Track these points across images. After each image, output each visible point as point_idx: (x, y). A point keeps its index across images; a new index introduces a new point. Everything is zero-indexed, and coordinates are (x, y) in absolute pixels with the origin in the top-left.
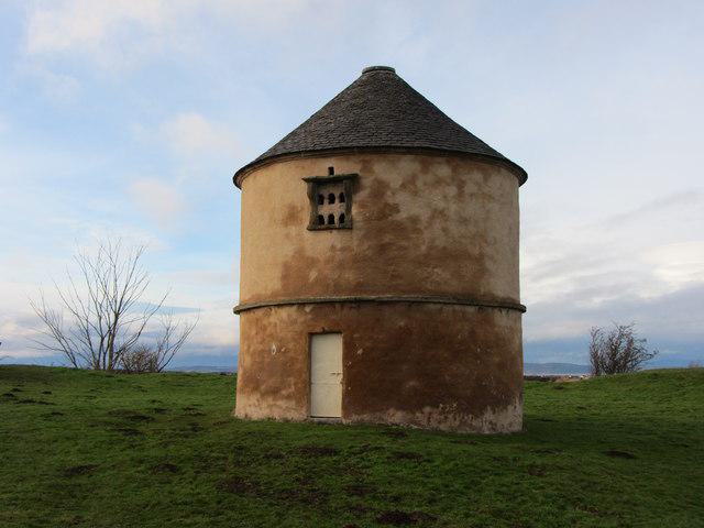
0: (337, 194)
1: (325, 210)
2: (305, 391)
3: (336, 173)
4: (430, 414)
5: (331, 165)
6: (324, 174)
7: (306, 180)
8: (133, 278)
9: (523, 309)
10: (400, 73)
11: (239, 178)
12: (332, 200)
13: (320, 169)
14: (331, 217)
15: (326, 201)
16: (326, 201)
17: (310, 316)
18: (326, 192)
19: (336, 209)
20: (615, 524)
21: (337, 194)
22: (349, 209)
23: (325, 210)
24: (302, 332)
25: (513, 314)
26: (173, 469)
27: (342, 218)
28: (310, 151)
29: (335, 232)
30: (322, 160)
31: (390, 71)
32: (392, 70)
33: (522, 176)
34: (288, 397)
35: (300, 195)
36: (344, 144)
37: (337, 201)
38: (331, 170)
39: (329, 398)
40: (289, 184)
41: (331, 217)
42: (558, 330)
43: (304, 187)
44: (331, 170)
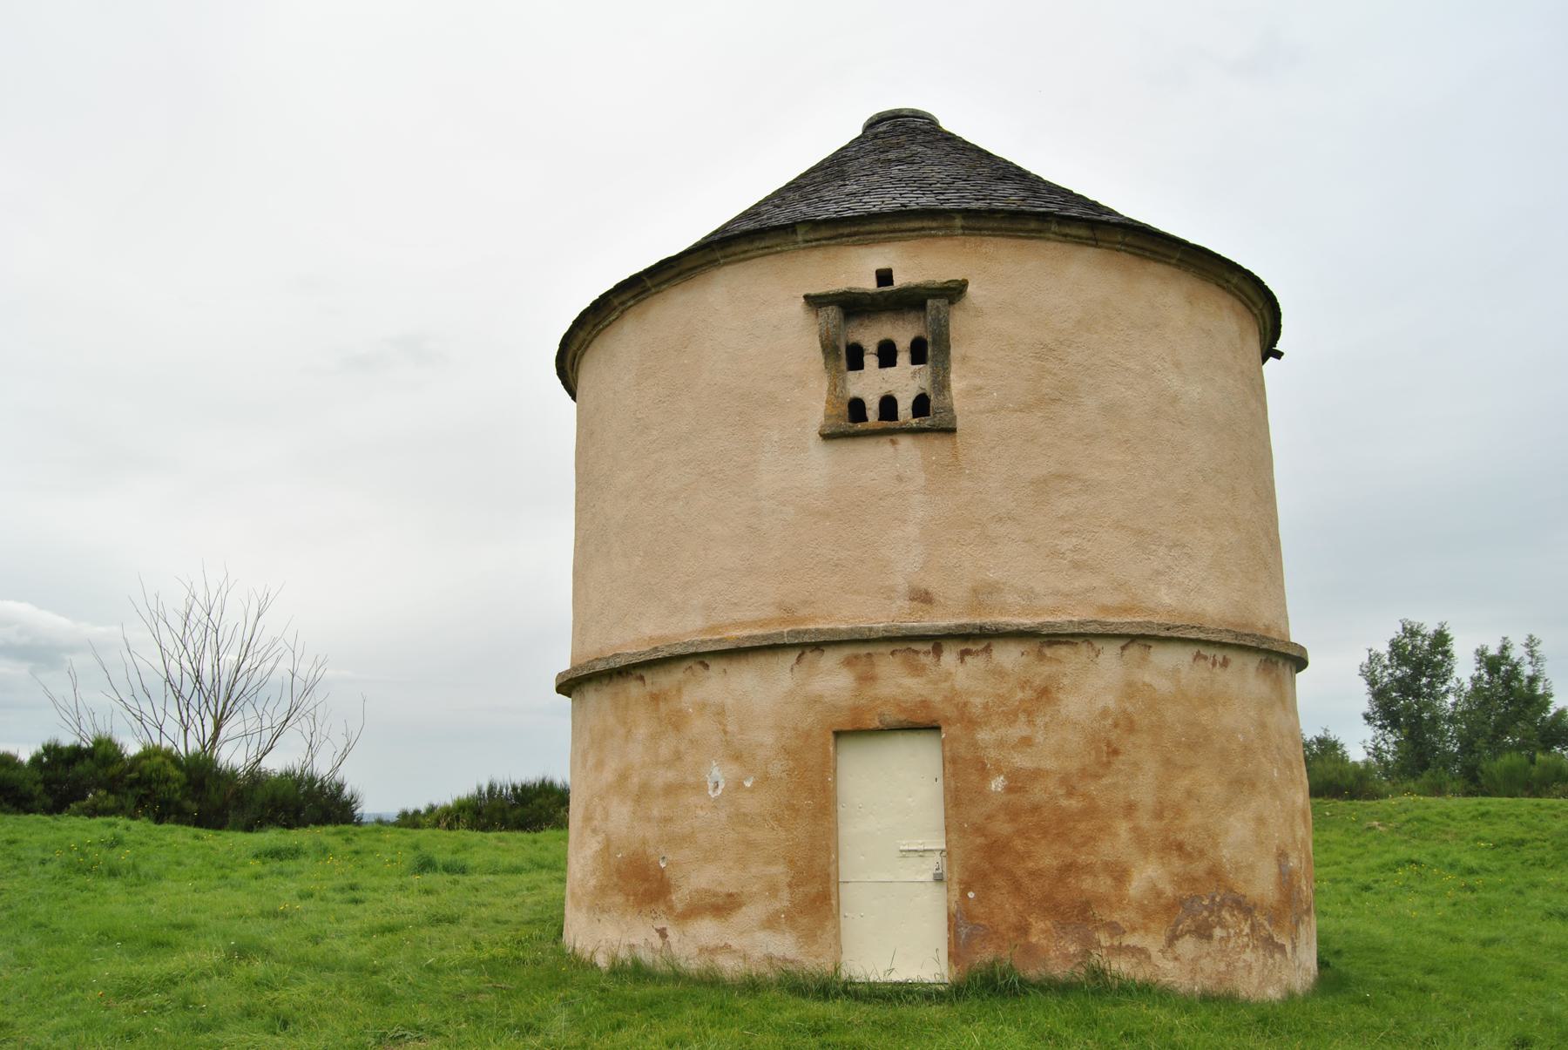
0: (903, 340)
1: (870, 384)
2: (815, 896)
3: (900, 280)
4: (1195, 960)
5: (883, 265)
6: (870, 284)
8: (248, 661)
11: (567, 686)
12: (887, 355)
13: (856, 269)
14: (888, 406)
15: (871, 361)
16: (871, 361)
18: (870, 336)
19: (905, 381)
22: (941, 384)
23: (870, 384)
24: (1216, 845)
26: (1018, 889)
27: (921, 405)
29: (905, 442)
30: (862, 251)
33: (1260, 308)
34: (771, 923)
35: (800, 338)
37: (903, 358)
38: (884, 277)
39: (897, 931)
40: (768, 313)
41: (888, 406)
42: (946, 974)
44: (884, 277)
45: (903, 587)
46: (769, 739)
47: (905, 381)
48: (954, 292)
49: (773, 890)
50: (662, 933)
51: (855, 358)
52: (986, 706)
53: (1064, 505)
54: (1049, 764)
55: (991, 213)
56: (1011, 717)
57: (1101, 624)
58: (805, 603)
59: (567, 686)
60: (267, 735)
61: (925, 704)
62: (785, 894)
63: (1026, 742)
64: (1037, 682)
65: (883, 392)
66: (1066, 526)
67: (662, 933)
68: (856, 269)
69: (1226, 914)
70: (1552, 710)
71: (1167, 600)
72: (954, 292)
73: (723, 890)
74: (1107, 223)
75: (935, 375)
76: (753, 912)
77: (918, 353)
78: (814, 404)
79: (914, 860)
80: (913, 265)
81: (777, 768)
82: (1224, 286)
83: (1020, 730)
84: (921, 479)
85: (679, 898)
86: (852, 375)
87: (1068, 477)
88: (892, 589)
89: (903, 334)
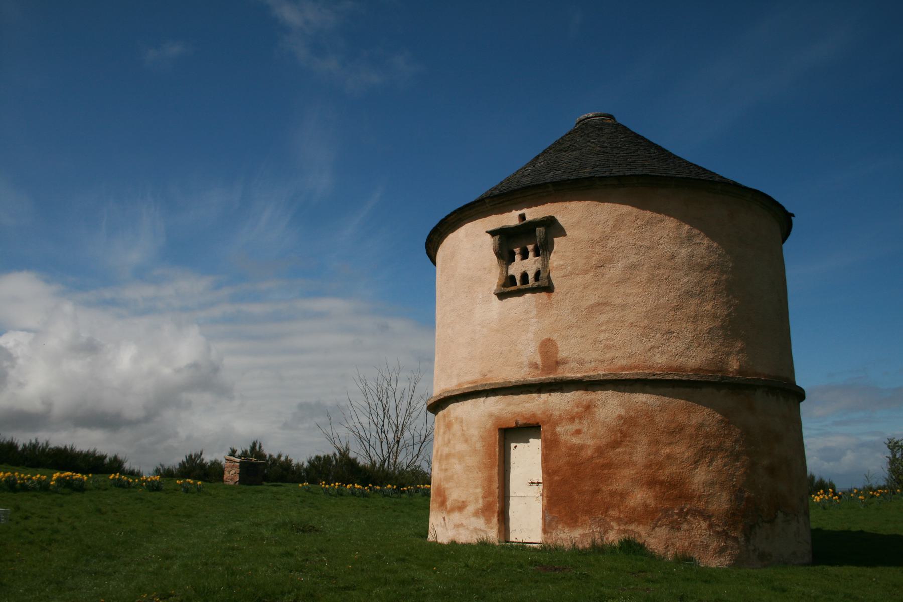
1: (517, 268)
3: (528, 218)
7: (493, 233)
9: (800, 395)
13: (511, 219)
14: (524, 276)
19: (529, 265)
38: (522, 217)
39: (528, 523)
41: (524, 276)
44: (522, 217)
45: (526, 363)
46: (476, 433)
49: (476, 500)
50: (444, 518)
52: (560, 416)
53: (603, 318)
54: (591, 442)
55: (577, 181)
56: (572, 419)
57: (615, 375)
58: (490, 371)
60: (417, 448)
61: (534, 416)
62: (481, 501)
63: (578, 432)
64: (585, 403)
66: (604, 328)
67: (444, 518)
68: (511, 219)
69: (334, 463)
71: (659, 361)
73: (461, 499)
75: (543, 261)
76: (471, 508)
79: (535, 487)
81: (479, 446)
83: (576, 426)
84: (534, 312)
85: (449, 504)
87: (605, 304)
88: (522, 363)
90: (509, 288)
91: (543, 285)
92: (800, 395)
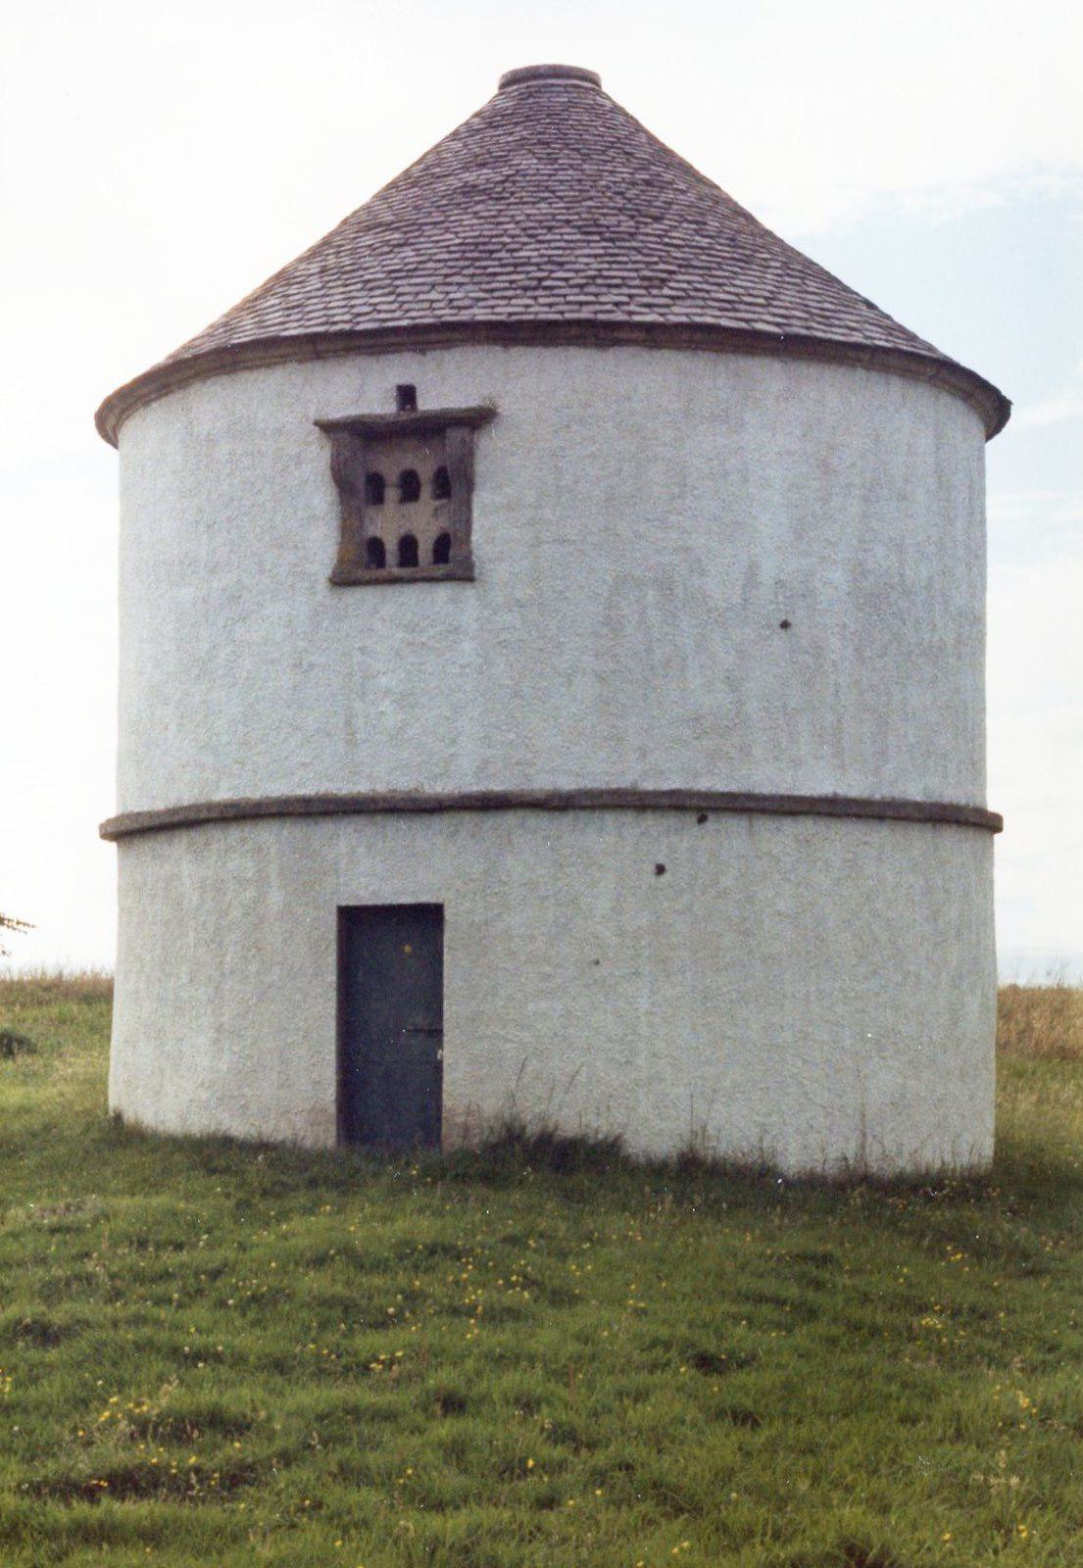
0: (426, 473)
1: (388, 523)
5: (405, 380)
7: (328, 428)
9: (991, 824)
10: (621, 88)
11: (128, 832)
12: (410, 489)
13: (363, 390)
14: (408, 545)
15: (392, 494)
16: (392, 494)
17: (1063, 1157)
18: (390, 465)
19: (424, 520)
20: (135, 1562)
21: (426, 473)
23: (388, 523)
25: (952, 843)
27: (443, 547)
28: (341, 334)
31: (578, 83)
32: (592, 79)
36: (448, 315)
37: (426, 492)
38: (407, 395)
41: (408, 545)
43: (318, 456)
44: (407, 395)
47: (424, 520)
48: (479, 419)
51: (376, 489)
59: (128, 832)
65: (403, 532)
70: (710, 1160)
72: (479, 419)
74: (924, 357)
77: (444, 485)
78: (321, 542)
80: (447, 384)
82: (966, 397)
86: (371, 512)
89: (424, 465)
90: (365, 563)
91: (448, 559)
92: (991, 824)
